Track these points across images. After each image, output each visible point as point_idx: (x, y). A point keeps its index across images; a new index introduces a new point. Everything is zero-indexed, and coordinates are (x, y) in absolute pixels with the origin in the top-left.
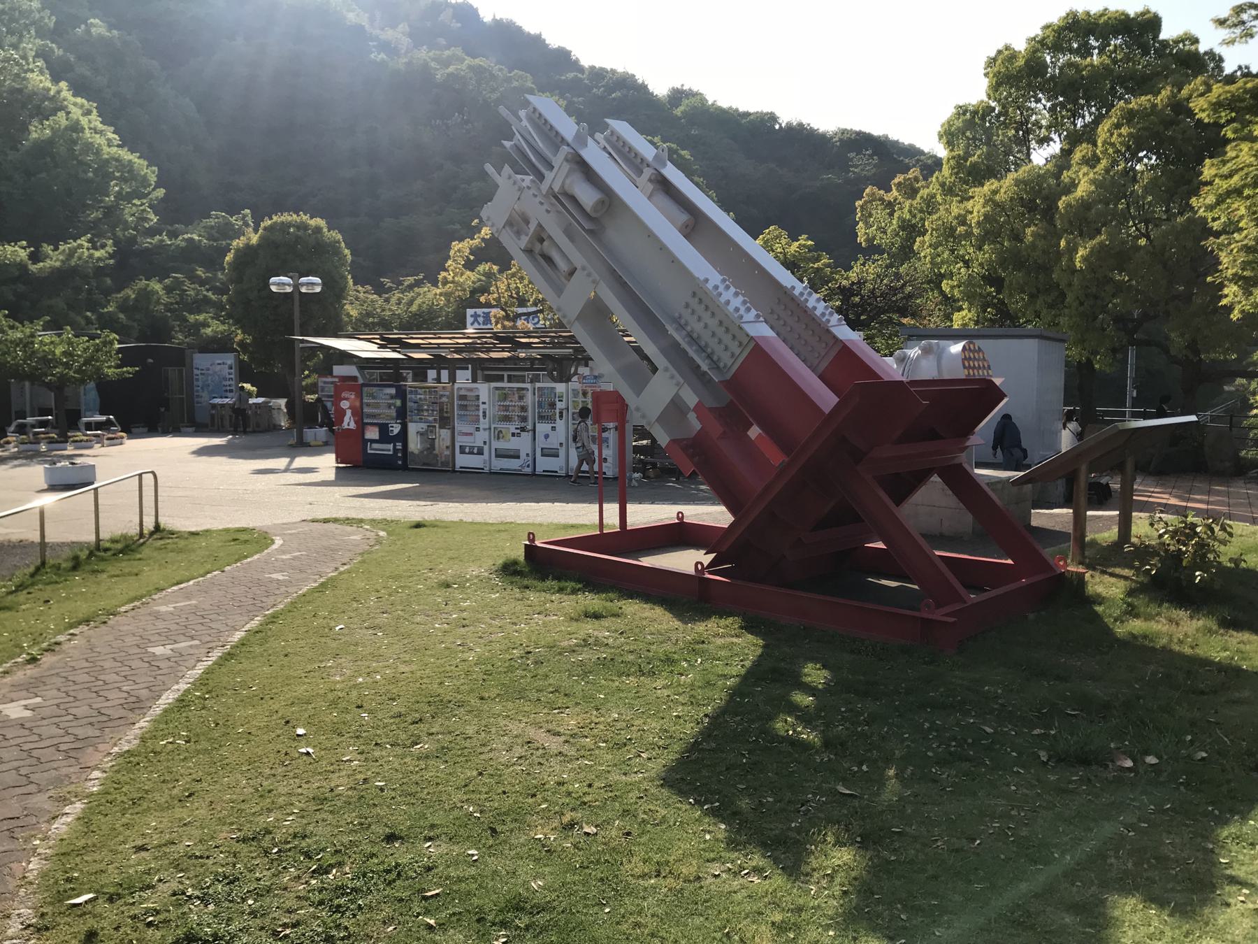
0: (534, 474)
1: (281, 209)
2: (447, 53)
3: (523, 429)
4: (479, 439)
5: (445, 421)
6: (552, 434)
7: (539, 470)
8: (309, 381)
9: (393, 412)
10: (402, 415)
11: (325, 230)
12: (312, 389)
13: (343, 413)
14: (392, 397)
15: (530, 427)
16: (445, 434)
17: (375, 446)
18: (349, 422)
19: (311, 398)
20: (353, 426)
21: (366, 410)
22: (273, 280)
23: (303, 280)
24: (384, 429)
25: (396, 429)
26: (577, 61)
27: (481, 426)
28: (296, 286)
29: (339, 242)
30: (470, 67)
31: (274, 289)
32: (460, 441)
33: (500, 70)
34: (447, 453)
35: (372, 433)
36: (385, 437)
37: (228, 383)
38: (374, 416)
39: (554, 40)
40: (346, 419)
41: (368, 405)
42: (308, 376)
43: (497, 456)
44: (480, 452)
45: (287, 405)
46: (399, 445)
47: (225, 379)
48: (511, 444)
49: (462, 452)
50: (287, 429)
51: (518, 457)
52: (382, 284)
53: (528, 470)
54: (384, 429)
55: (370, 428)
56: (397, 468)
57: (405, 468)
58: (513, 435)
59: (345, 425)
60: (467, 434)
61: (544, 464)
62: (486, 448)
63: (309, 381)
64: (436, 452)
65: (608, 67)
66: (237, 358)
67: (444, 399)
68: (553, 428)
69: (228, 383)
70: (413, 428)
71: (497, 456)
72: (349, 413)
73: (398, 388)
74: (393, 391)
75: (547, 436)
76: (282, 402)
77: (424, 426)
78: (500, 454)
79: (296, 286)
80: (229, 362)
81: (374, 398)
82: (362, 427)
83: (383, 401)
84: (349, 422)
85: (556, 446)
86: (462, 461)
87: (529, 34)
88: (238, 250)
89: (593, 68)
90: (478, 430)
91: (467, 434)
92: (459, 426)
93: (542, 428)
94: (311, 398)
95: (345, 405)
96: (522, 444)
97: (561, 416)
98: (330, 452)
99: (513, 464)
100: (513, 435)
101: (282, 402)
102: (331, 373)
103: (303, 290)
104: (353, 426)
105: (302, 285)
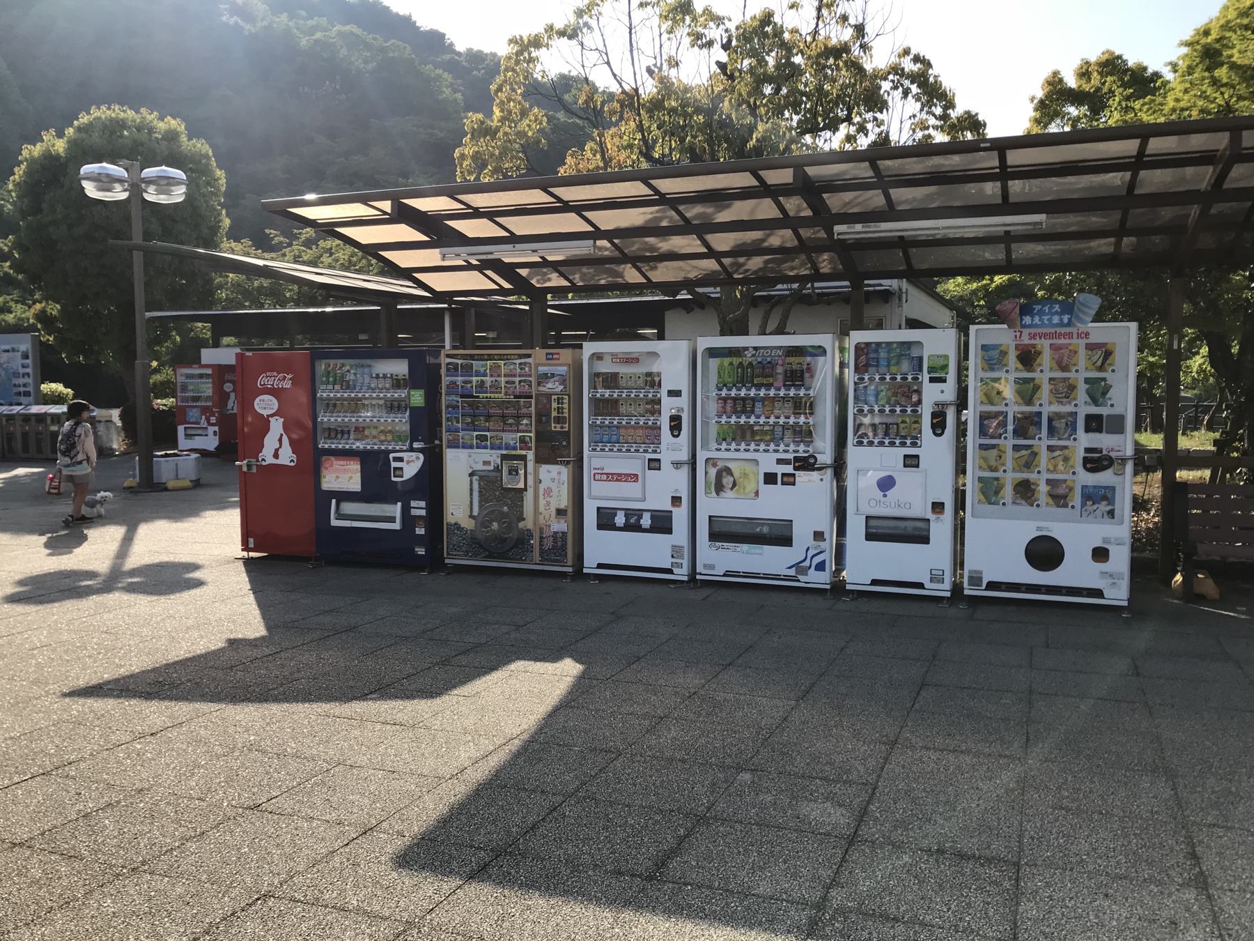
0: (838, 588)
1: (108, 101)
2: (310, 23)
3: (805, 464)
4: (661, 488)
5: (557, 445)
6: (905, 478)
7: (857, 574)
8: (157, 378)
9: (401, 422)
10: (427, 429)
11: (184, 138)
12: (166, 389)
13: (263, 425)
14: (397, 383)
15: (826, 457)
16: (554, 478)
17: (349, 508)
18: (276, 448)
19: (161, 403)
20: (287, 457)
21: (324, 418)
22: (86, 169)
23: (149, 172)
24: (375, 466)
25: (410, 466)
26: (452, 44)
27: (666, 457)
28: (136, 189)
29: (207, 157)
30: (340, 33)
31: (91, 190)
32: (597, 495)
33: (375, 39)
34: (561, 526)
35: (343, 477)
36: (378, 482)
37: (21, 381)
38: (342, 432)
39: (425, 22)
40: (270, 442)
41: (331, 406)
42: (156, 371)
43: (714, 536)
44: (662, 524)
45: (122, 417)
46: (419, 508)
47: (16, 375)
48: (772, 504)
49: (606, 520)
50: (123, 454)
51: (786, 541)
52: (268, 238)
53: (821, 579)
54: (375, 466)
55: (337, 464)
56: (416, 565)
57: (434, 562)
58: (770, 479)
59: (267, 456)
60: (619, 477)
61: (868, 564)
62: (680, 517)
63: (157, 378)
64: (528, 523)
65: (487, 50)
66: (36, 340)
67: (553, 386)
68: (911, 462)
69: (21, 381)
70: (459, 467)
71: (714, 536)
72: (277, 426)
73: (416, 361)
74: (400, 368)
75: (886, 484)
76: (115, 414)
77: (493, 456)
78: (726, 532)
79: (136, 189)
80: (23, 348)
81: (348, 386)
82: (312, 458)
83: (372, 399)
84: (276, 448)
85: (919, 508)
86: (602, 549)
87: (397, 14)
88: (32, 161)
89: (470, 50)
90: (654, 464)
91: (619, 477)
92: (593, 461)
93: (869, 464)
94: (161, 403)
95: (265, 405)
96: (805, 504)
97: (938, 426)
98: (221, 505)
99: (768, 561)
100: (770, 479)
101: (115, 414)
102: (197, 360)
103: (151, 196)
104: (287, 457)
105: (149, 182)
